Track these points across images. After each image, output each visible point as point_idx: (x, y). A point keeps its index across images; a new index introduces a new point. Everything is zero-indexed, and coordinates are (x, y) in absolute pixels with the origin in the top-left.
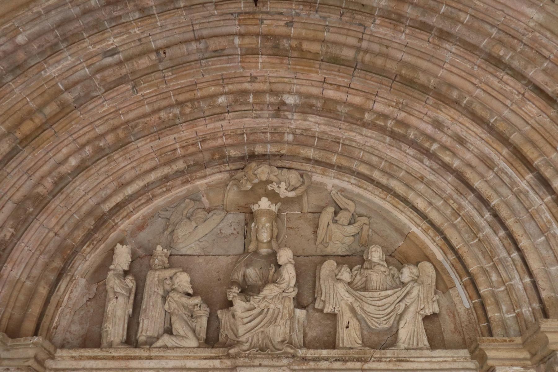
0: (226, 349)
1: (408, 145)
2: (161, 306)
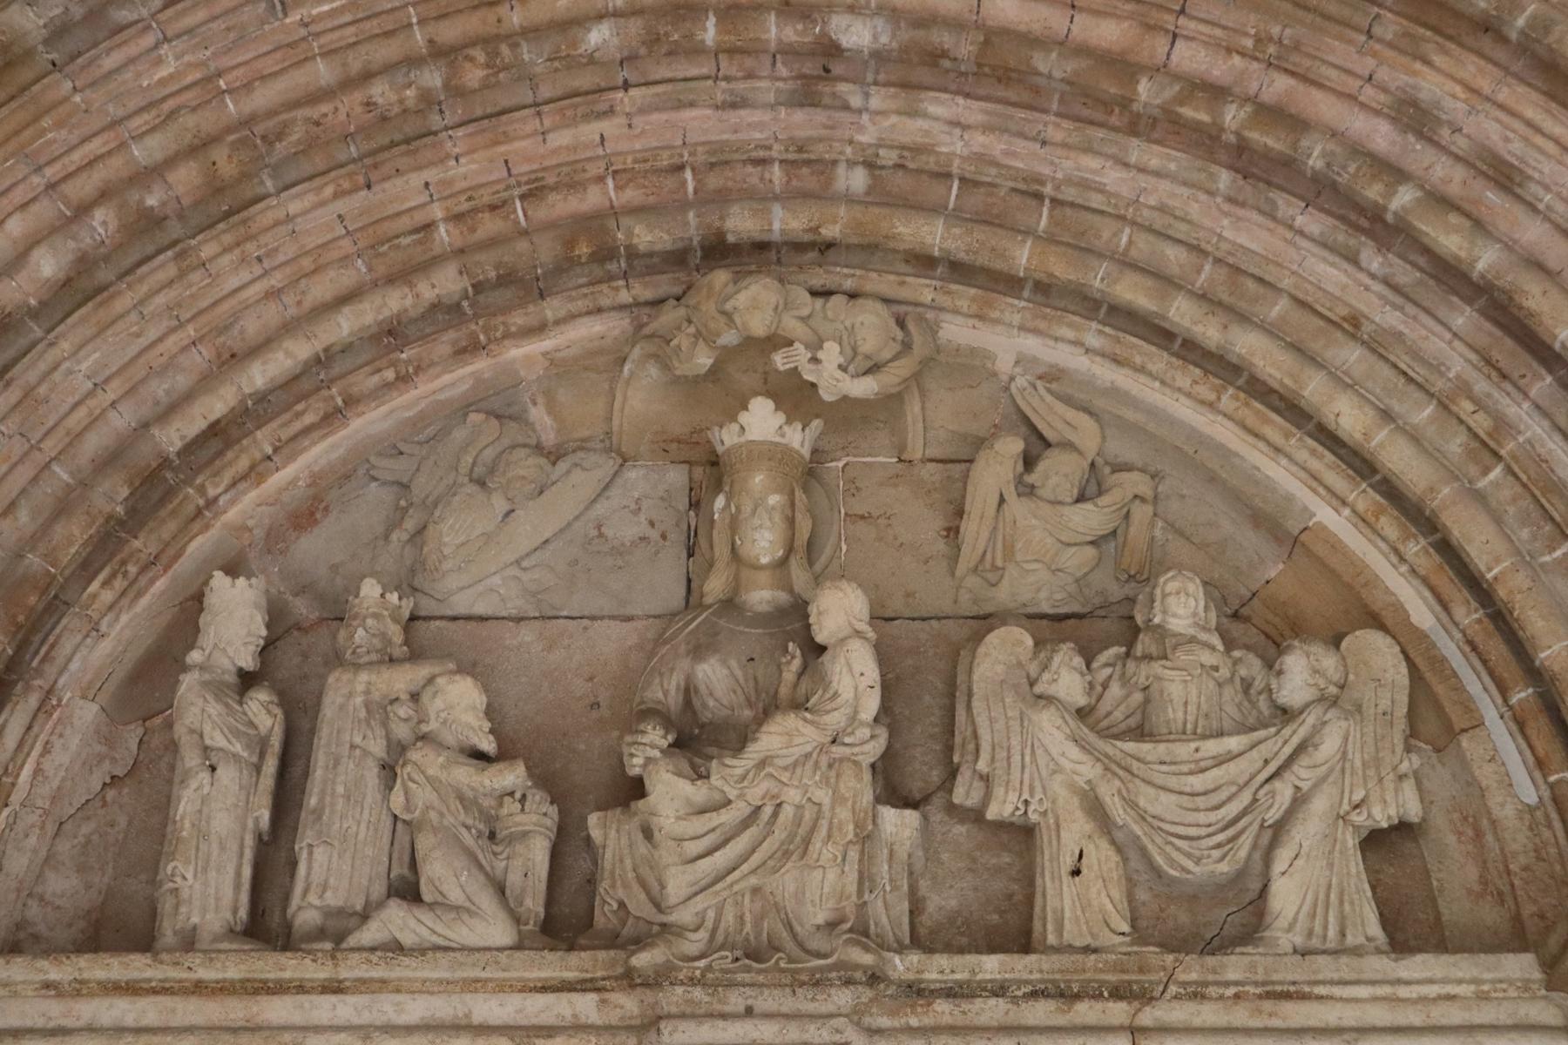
0: (622, 954)
1: (1302, 198)
2: (379, 797)
